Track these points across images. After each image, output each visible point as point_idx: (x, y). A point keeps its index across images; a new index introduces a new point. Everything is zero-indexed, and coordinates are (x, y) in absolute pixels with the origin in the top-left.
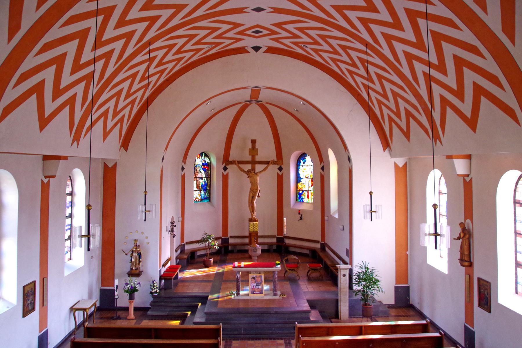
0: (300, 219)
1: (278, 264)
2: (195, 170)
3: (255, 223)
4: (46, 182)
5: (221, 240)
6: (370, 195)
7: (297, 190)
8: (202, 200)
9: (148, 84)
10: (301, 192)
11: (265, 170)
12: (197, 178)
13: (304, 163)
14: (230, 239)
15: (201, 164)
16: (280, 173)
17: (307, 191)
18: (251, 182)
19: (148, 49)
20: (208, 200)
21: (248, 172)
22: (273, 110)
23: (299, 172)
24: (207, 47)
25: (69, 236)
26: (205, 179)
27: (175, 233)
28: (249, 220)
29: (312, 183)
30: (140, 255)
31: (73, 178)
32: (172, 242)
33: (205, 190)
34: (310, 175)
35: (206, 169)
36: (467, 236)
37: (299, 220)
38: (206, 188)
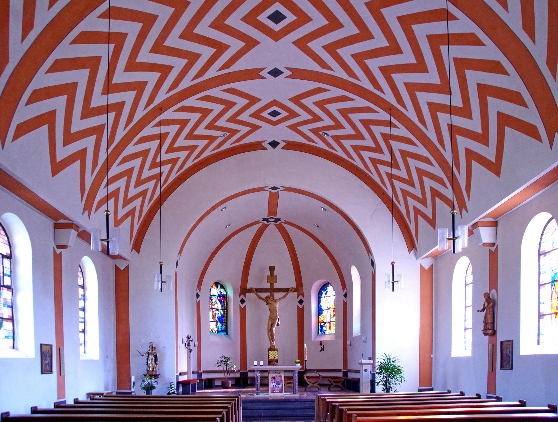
0: (322, 350)
1: (298, 363)
2: (211, 301)
4: (58, 253)
5: (239, 373)
6: (392, 266)
7: (318, 323)
8: (218, 332)
9: (161, 174)
10: (322, 324)
11: (284, 297)
12: (212, 308)
13: (326, 294)
14: (248, 373)
15: (217, 295)
16: (301, 306)
17: (329, 322)
18: (270, 310)
19: (158, 120)
20: (225, 333)
22: (292, 231)
23: (321, 304)
24: (221, 136)
25: (82, 329)
26: (222, 311)
27: (191, 348)
29: (334, 313)
30: (156, 357)
31: (85, 272)
32: (189, 358)
33: (222, 322)
34: (333, 306)
35: (222, 300)
36: (491, 304)
37: (320, 351)
38: (223, 321)
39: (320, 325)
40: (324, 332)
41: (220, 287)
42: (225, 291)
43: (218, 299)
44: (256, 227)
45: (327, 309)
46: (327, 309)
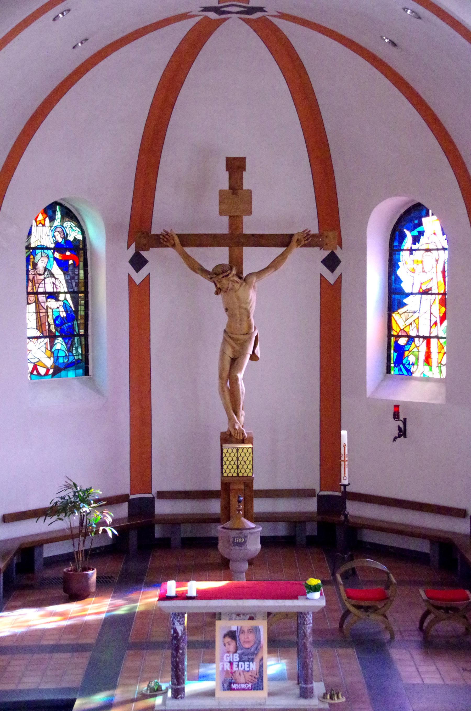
0: (399, 436)
2: (30, 267)
3: (243, 449)
7: (390, 336)
10: (402, 341)
12: (37, 293)
13: (416, 240)
14: (156, 499)
15: (53, 246)
16: (331, 278)
17: (424, 337)
18: (227, 310)
21: (217, 274)
23: (400, 273)
26: (68, 296)
28: (221, 439)
29: (443, 309)
35: (71, 262)
37: (395, 439)
38: (74, 330)
39: (396, 342)
40: (408, 370)
41: (63, 217)
42: (80, 226)
43: (55, 259)
44: (188, 24)
45: (419, 293)
46: (419, 293)
